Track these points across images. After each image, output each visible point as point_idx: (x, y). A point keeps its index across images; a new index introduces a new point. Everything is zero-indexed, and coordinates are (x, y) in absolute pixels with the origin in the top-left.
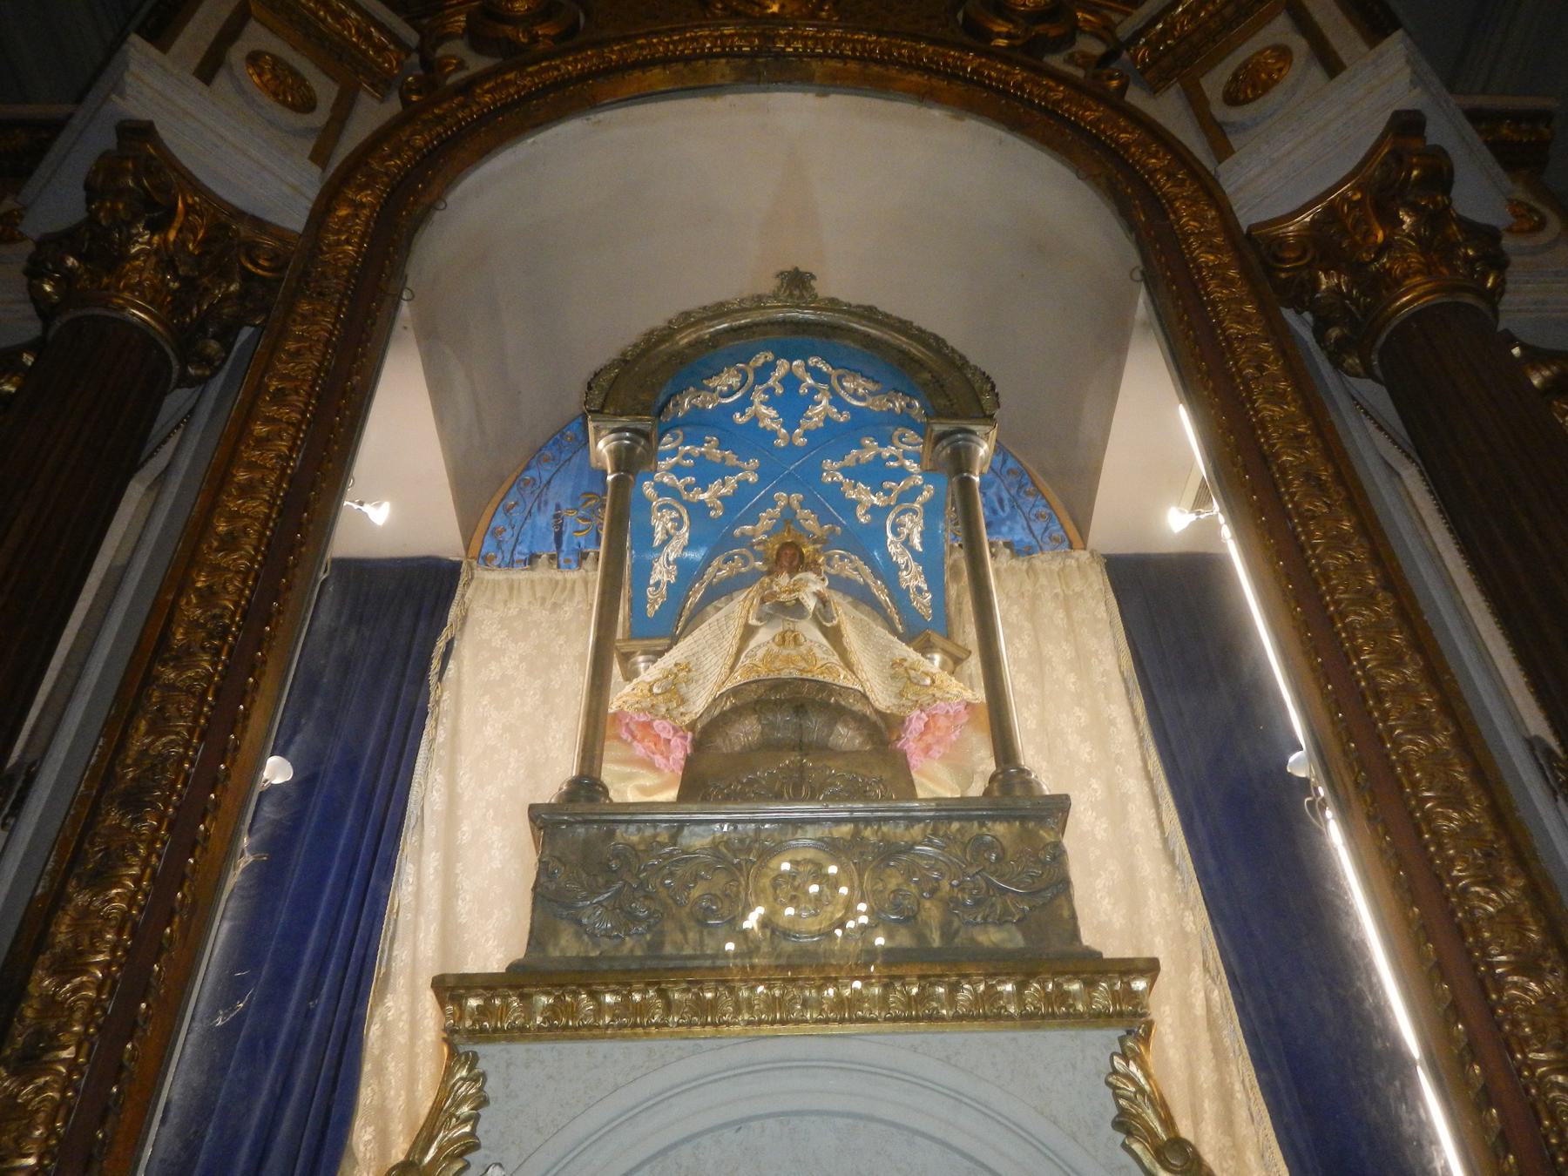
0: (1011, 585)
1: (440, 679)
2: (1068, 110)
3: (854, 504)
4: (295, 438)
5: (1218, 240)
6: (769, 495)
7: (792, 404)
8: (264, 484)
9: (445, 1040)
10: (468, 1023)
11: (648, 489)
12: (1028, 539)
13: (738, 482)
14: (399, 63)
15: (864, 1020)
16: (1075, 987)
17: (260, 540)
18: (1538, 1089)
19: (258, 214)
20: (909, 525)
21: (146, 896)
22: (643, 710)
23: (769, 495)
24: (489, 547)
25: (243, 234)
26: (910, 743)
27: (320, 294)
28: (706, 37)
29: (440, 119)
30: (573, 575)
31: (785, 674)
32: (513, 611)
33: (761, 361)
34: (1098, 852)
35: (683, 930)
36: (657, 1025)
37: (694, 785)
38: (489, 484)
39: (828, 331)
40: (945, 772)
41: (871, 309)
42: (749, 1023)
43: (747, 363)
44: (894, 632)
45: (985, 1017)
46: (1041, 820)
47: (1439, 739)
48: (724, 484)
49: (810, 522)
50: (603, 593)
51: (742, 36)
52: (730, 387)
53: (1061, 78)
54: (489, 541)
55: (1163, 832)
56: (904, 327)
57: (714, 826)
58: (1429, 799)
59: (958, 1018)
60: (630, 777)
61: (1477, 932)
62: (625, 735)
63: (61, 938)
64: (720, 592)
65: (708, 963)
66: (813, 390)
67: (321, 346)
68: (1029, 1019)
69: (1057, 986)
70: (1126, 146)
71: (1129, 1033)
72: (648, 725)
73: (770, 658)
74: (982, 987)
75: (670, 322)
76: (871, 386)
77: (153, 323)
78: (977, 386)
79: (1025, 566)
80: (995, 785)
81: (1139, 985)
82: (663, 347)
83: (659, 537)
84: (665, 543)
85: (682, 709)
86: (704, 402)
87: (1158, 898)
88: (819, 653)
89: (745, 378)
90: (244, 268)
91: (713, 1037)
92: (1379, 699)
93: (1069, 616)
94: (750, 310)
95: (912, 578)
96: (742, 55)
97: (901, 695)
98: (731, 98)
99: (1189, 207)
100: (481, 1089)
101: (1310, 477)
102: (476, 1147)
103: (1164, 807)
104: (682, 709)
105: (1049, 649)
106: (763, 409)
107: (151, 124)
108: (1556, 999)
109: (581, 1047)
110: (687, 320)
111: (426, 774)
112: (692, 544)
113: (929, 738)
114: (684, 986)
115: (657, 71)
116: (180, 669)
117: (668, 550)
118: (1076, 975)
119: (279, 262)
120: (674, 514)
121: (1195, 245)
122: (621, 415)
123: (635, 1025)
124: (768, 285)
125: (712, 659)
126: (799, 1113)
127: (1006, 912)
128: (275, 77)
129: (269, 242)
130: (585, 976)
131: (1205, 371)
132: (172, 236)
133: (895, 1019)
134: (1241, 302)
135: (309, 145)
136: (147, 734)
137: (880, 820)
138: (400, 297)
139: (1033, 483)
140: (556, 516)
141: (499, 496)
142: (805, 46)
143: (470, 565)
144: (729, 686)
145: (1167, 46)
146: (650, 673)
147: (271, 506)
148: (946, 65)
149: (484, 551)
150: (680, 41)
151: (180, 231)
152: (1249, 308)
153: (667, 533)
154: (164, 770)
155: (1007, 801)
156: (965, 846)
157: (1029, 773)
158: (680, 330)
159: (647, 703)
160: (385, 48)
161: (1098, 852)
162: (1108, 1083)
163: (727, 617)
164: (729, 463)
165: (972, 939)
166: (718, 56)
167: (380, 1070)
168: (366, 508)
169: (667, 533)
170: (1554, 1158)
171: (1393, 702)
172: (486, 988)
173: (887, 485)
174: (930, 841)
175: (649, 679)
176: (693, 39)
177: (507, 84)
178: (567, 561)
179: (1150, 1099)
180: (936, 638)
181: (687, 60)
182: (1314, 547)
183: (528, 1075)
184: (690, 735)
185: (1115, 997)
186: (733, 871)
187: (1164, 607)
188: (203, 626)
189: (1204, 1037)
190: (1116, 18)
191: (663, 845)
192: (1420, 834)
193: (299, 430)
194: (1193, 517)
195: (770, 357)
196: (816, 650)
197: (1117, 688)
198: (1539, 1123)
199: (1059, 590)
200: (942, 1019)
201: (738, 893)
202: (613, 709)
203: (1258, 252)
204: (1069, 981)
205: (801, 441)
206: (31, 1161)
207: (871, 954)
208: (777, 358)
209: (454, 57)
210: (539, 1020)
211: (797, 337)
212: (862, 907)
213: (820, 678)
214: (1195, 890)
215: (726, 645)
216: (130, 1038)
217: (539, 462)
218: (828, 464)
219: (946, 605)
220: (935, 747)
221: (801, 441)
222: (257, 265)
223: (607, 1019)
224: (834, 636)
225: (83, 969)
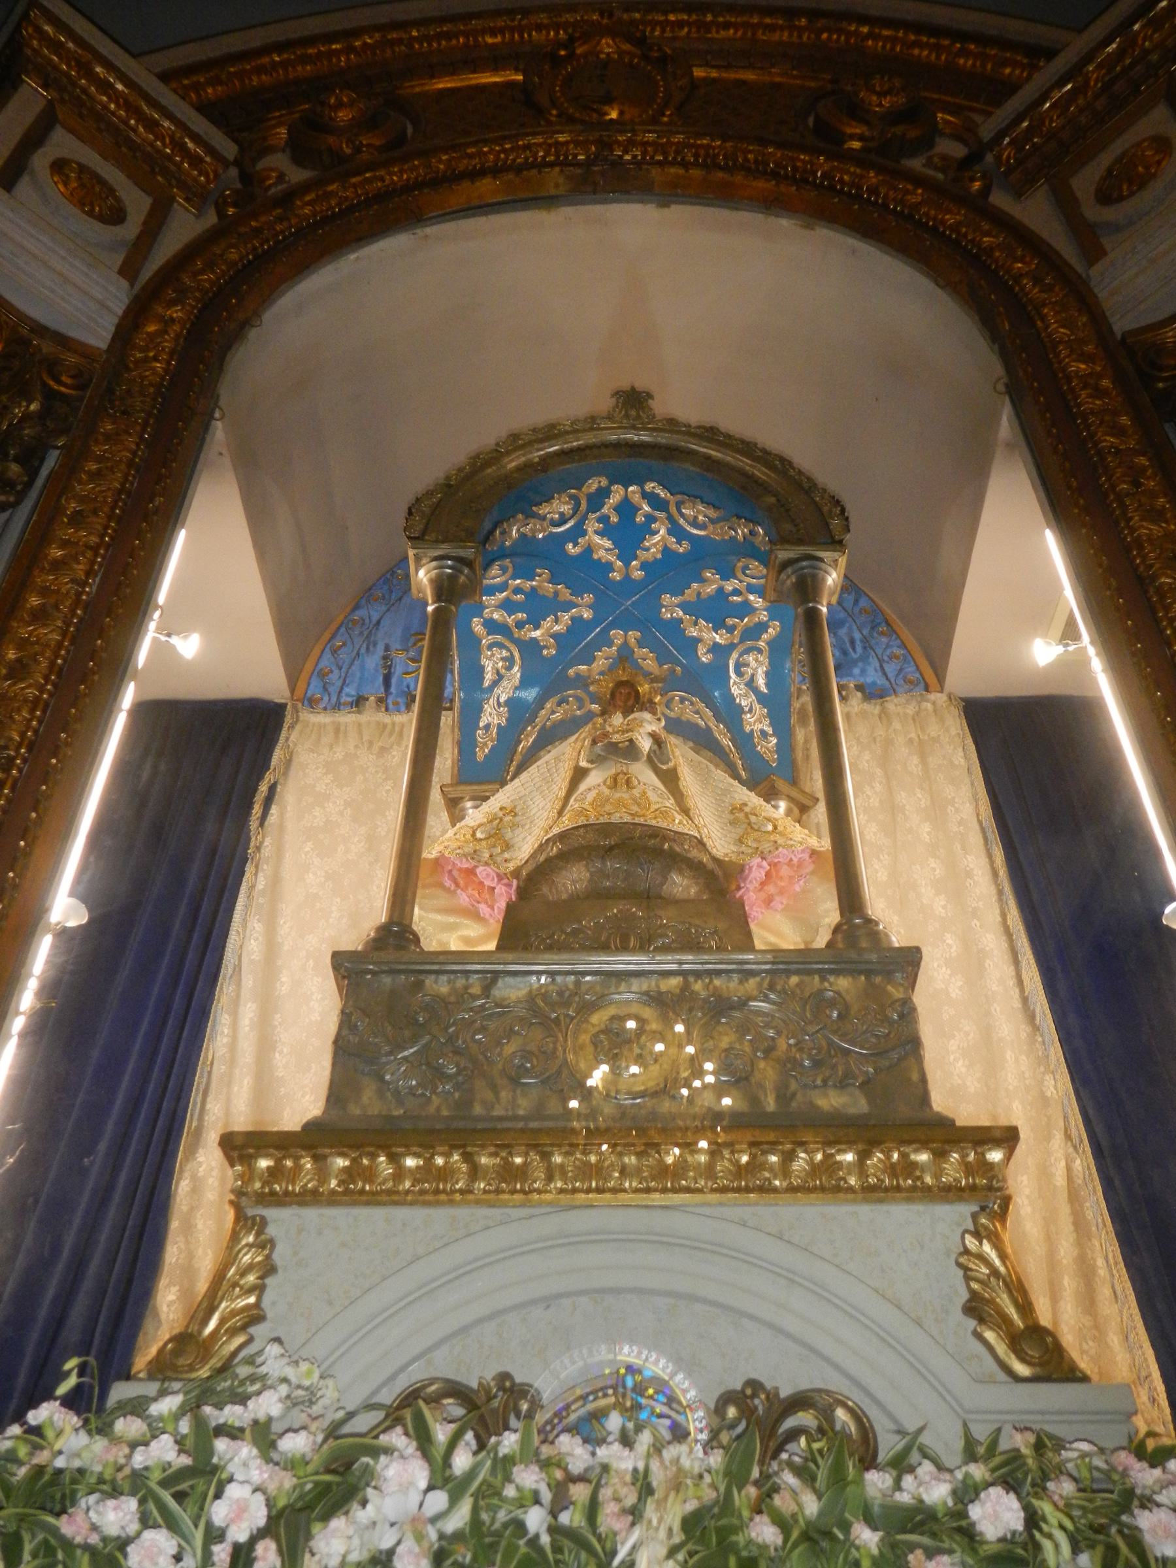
0: (862, 729)
1: (262, 825)
2: (927, 214)
3: (698, 640)
5: (1090, 348)
7: (628, 534)
8: (58, 610)
9: (231, 1202)
10: (258, 1185)
11: (477, 626)
12: (881, 681)
13: (572, 619)
14: (216, 175)
15: (688, 1190)
16: (923, 1157)
19: (63, 329)
20: (753, 664)
22: (465, 855)
23: (605, 631)
24: (315, 689)
25: (44, 351)
26: (750, 894)
27: (124, 413)
28: (540, 145)
29: (257, 232)
30: (400, 719)
31: (615, 818)
33: (595, 486)
35: (494, 1088)
36: (461, 1192)
37: (517, 934)
39: (669, 453)
40: (788, 921)
43: (579, 488)
44: (736, 776)
45: (823, 1189)
48: (557, 621)
49: (648, 661)
51: (577, 144)
52: (562, 514)
53: (918, 181)
55: (1022, 990)
56: (747, 448)
57: (534, 977)
59: (792, 1189)
60: (451, 928)
62: (448, 883)
64: (549, 737)
65: (521, 1125)
66: (650, 519)
67: (123, 467)
68: (872, 1192)
69: (904, 1156)
70: (990, 250)
71: (983, 1209)
72: (471, 872)
73: (600, 801)
76: (712, 513)
78: (825, 509)
80: (839, 937)
81: (995, 1156)
82: (489, 470)
83: (489, 677)
84: (495, 683)
85: (506, 855)
86: (534, 531)
87: (1017, 1060)
88: (652, 796)
89: (577, 505)
90: (44, 384)
91: (523, 1205)
94: (585, 431)
95: (756, 721)
96: (579, 164)
97: (740, 841)
98: (566, 212)
99: (1057, 313)
100: (268, 1257)
103: (1024, 964)
104: (506, 855)
105: (902, 797)
106: (597, 539)
109: (378, 1214)
110: (515, 441)
111: (245, 922)
112: (524, 683)
113: (771, 889)
114: (492, 1149)
115: (487, 181)
118: (924, 1144)
119: (82, 381)
120: (505, 653)
122: (443, 542)
123: (437, 1192)
124: (605, 403)
125: (538, 805)
126: (616, 1291)
127: (848, 1074)
128: (82, 185)
129: (72, 359)
130: (386, 1136)
131: (1078, 496)
133: (723, 1190)
135: (119, 259)
137: (709, 973)
138: (212, 418)
139: (888, 624)
140: (385, 658)
141: (327, 635)
142: (644, 153)
144: (556, 830)
145: (1034, 144)
146: (474, 815)
147: (64, 634)
148: (795, 169)
149: (309, 693)
150: (512, 149)
152: (1125, 420)
153: (498, 673)
155: (853, 955)
156: (804, 1002)
157: (877, 924)
158: (508, 453)
159: (469, 849)
160: (202, 160)
162: (959, 1265)
164: (561, 598)
165: (811, 1104)
166: (551, 165)
167: (188, 1228)
169: (498, 673)
172: (277, 1148)
174: (766, 996)
175: (472, 824)
176: (527, 147)
177: (328, 195)
178: (396, 704)
179: (1004, 1282)
180: (781, 785)
181: (519, 170)
184: (515, 882)
185: (969, 1169)
186: (551, 1026)
187: (1030, 759)
189: (1065, 1210)
190: (977, 118)
191: (475, 998)
194: (1060, 649)
195: (604, 482)
196: (650, 794)
197: (975, 839)
199: (913, 735)
200: (775, 1190)
201: (555, 1049)
202: (430, 852)
204: (916, 1151)
205: (638, 574)
207: (717, 1116)
208: (612, 483)
209: (272, 170)
210: (333, 1183)
212: (709, 1066)
213: (653, 823)
214: (1056, 1053)
215: (555, 788)
217: (368, 601)
218: (667, 599)
219: (792, 749)
220: (777, 898)
221: (638, 574)
222: (60, 383)
223: (407, 1184)
224: (670, 779)
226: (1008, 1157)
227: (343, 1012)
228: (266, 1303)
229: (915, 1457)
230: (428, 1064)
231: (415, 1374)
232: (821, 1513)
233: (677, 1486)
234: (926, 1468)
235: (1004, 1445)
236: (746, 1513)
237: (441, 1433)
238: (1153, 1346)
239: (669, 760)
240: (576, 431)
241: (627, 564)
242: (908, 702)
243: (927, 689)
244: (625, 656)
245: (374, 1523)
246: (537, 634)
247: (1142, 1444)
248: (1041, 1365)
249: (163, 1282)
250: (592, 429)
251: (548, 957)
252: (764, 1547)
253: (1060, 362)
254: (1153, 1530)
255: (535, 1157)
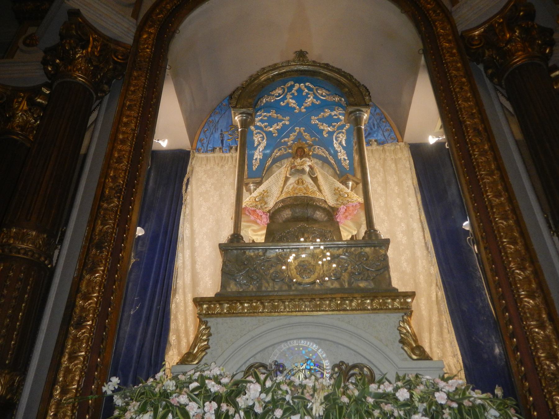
1: (186, 192)
3: (323, 130)
4: (136, 123)
6: (293, 128)
7: (300, 98)
11: (252, 128)
12: (383, 138)
13: (283, 124)
15: (323, 311)
17: (129, 159)
18: (529, 332)
20: (341, 137)
21: (106, 276)
22: (253, 207)
26: (340, 218)
30: (228, 155)
31: (299, 195)
32: (209, 168)
34: (403, 247)
35: (268, 283)
36: (261, 312)
37: (270, 235)
38: (199, 124)
39: (313, 73)
40: (350, 229)
41: (327, 65)
42: (288, 312)
43: (284, 85)
45: (361, 310)
46: (380, 247)
47: (511, 222)
48: (278, 125)
49: (307, 136)
50: (239, 172)
52: (279, 94)
54: (202, 134)
55: (425, 240)
56: (339, 71)
58: (505, 242)
59: (352, 310)
60: (249, 227)
61: (516, 284)
62: (247, 213)
63: (83, 288)
71: (405, 314)
72: (255, 211)
73: (294, 189)
74: (360, 301)
75: (258, 72)
76: (327, 92)
77: (87, 83)
79: (381, 148)
81: (409, 300)
83: (256, 143)
86: (270, 100)
87: (422, 263)
88: (310, 187)
90: (114, 59)
92: (492, 209)
93: (396, 166)
94: (285, 66)
95: (342, 155)
97: (337, 200)
101: (476, 129)
102: (209, 348)
103: (426, 232)
105: (389, 178)
106: (291, 100)
107: (79, 10)
108: (538, 306)
110: (264, 71)
111: (183, 224)
113: (347, 214)
116: (109, 204)
117: (259, 147)
118: (389, 297)
120: (261, 136)
121: (442, 40)
123: (254, 313)
124: (291, 56)
125: (275, 188)
127: (369, 276)
130: (238, 298)
132: (89, 49)
133: (333, 310)
134: (457, 62)
135: (131, 10)
136: (101, 224)
139: (386, 118)
140: (221, 134)
143: (193, 152)
144: (281, 198)
151: (92, 48)
154: (107, 236)
155: (370, 242)
158: (262, 75)
159: (254, 204)
161: (403, 247)
162: (398, 329)
163: (280, 173)
164: (279, 118)
167: (176, 318)
168: (160, 142)
170: (532, 353)
171: (496, 209)
173: (333, 124)
180: (350, 176)
182: (475, 155)
183: (222, 326)
185: (401, 304)
188: (114, 189)
192: (501, 253)
193: (137, 120)
197: (412, 191)
198: (529, 342)
199: (393, 157)
200: (348, 310)
202: (244, 206)
203: (464, 41)
206: (83, 353)
210: (225, 311)
211: (301, 76)
213: (311, 196)
214: (434, 260)
216: (107, 319)
218: (313, 117)
219: (353, 164)
222: (118, 58)
223: (246, 311)
224: (315, 180)
225: (91, 298)
226: (412, 300)
227: (223, 261)
228: (210, 344)
229: (384, 380)
230: (249, 276)
231: (252, 361)
232: (359, 395)
233: (323, 389)
234: (387, 383)
235: (407, 378)
236: (340, 395)
237: (262, 377)
238: (459, 347)
239: (315, 174)
240: (283, 66)
241: (300, 107)
242: (391, 146)
243: (398, 141)
244: (300, 137)
245: (247, 399)
246: (271, 129)
247: (443, 376)
248: (419, 356)
249: (171, 334)
250: (288, 65)
251: (282, 244)
252: (344, 403)
253: (440, 43)
254: (438, 397)
255: (281, 304)
